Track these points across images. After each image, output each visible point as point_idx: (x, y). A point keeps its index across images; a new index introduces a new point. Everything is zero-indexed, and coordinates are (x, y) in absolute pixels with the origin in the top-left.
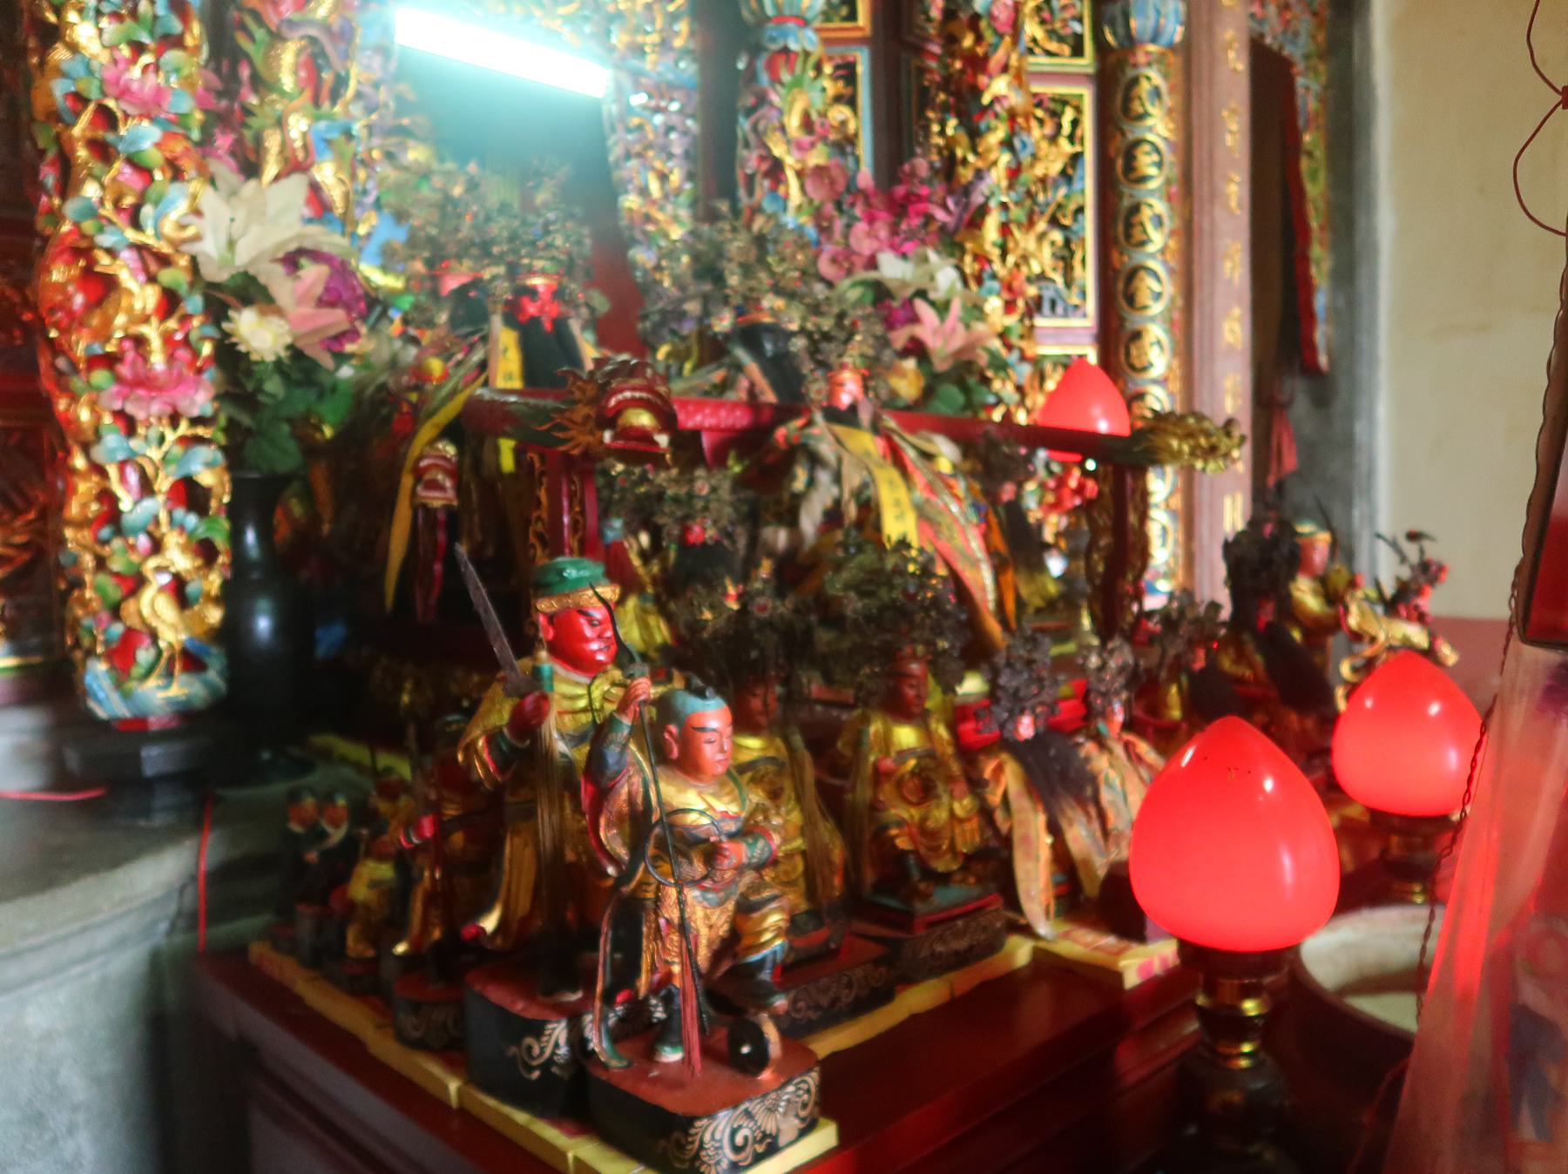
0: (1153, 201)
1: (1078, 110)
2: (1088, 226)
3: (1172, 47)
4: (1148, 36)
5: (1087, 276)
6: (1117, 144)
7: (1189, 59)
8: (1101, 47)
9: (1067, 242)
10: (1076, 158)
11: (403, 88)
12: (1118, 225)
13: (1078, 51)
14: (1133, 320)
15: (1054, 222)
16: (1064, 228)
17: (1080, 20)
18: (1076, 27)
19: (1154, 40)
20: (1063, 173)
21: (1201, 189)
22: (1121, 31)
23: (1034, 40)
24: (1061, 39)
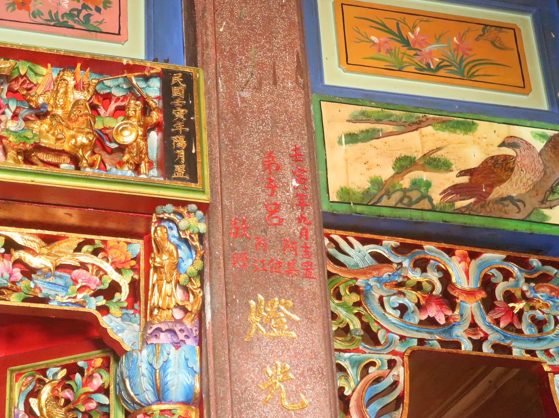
4: (150, 396)
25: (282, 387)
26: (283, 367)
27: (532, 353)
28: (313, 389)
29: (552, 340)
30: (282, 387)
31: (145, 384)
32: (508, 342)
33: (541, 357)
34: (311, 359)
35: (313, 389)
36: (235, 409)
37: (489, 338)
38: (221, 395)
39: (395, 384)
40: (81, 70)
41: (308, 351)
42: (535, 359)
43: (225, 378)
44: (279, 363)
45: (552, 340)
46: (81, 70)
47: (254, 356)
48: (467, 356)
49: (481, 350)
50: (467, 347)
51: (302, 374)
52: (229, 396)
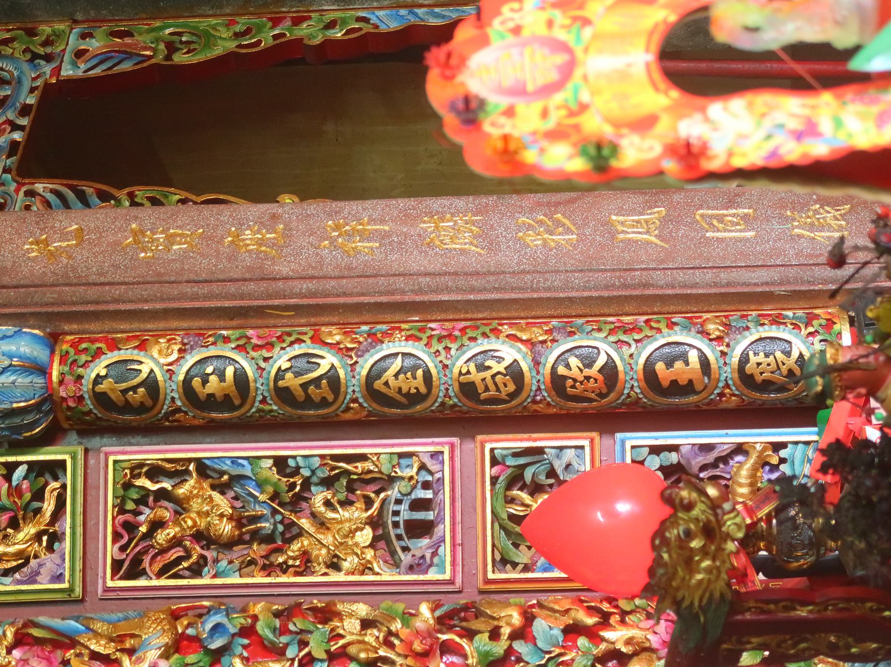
0: (460, 364)
1: (136, 469)
2: (306, 452)
3: (53, 340)
4: (39, 381)
5: (379, 451)
6: (192, 416)
7: (64, 316)
8: (48, 438)
9: (328, 483)
10: (203, 469)
11: (40, 653)
12: (306, 410)
13: (55, 469)
14: (445, 388)
15: (298, 501)
16: (307, 484)
17: (11, 468)
18: (20, 472)
19: (43, 371)
20: (222, 488)
21: (254, 293)
22: (28, 419)
23: (38, 537)
24: (39, 495)
25: (56, 245)
26: (31, 243)
27: (32, 90)
28: (61, 222)
29: (21, 72)
30: (56, 245)
31: (23, 380)
32: (18, 105)
33: (39, 83)
34: (24, 222)
35: (61, 222)
36: (75, 281)
37: (11, 118)
38: (55, 296)
39: (53, 191)
40: (515, 361)
41: (15, 224)
42: (40, 89)
43: (35, 292)
44: (26, 247)
45: (21, 72)
46: (515, 361)
47: (13, 266)
48: (29, 139)
49: (25, 126)
50: (17, 136)
51: (42, 230)
52: (58, 289)
